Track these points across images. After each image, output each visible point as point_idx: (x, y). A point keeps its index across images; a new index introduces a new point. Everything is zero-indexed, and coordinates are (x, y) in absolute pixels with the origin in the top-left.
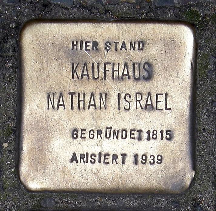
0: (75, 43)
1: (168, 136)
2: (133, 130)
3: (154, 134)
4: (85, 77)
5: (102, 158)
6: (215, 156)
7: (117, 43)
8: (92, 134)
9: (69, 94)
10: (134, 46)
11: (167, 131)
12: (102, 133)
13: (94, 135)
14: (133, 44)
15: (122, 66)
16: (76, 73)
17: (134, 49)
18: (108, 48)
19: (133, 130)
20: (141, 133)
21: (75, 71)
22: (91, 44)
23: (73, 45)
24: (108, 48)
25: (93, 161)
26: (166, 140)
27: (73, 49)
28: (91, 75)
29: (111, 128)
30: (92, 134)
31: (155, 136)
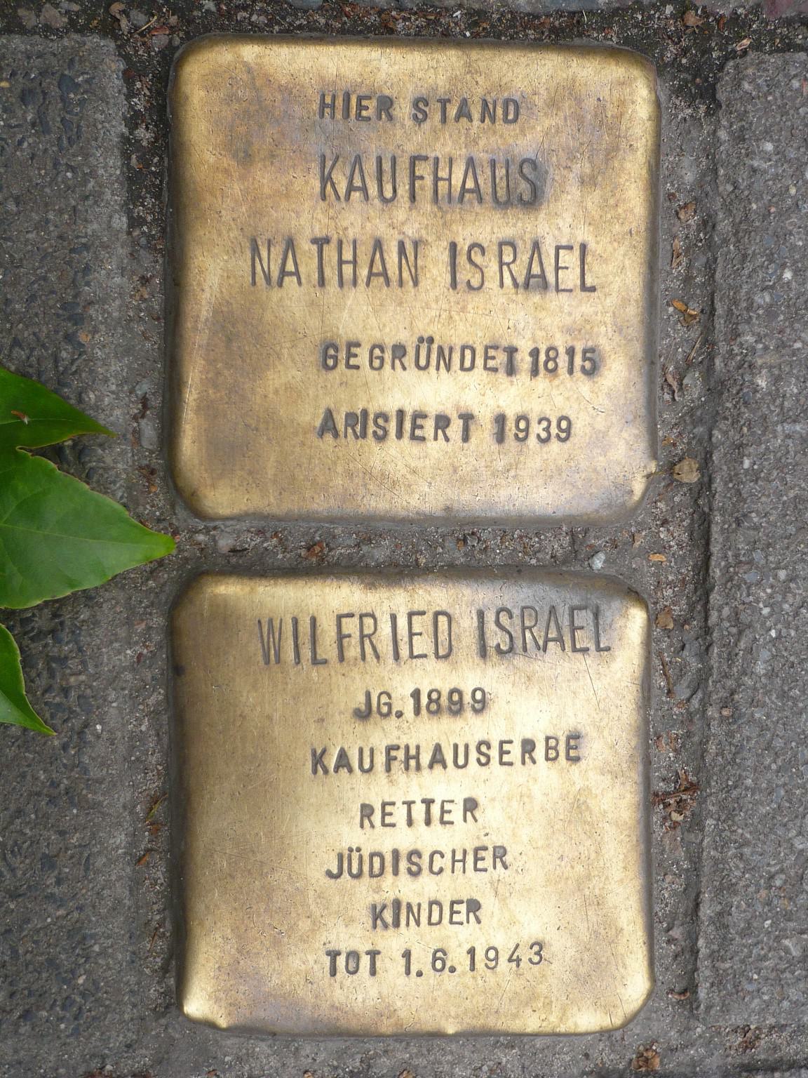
1: (588, 365)
3: (548, 359)
18: (420, 116)
24: (420, 116)
28: (373, 190)
29: (431, 340)
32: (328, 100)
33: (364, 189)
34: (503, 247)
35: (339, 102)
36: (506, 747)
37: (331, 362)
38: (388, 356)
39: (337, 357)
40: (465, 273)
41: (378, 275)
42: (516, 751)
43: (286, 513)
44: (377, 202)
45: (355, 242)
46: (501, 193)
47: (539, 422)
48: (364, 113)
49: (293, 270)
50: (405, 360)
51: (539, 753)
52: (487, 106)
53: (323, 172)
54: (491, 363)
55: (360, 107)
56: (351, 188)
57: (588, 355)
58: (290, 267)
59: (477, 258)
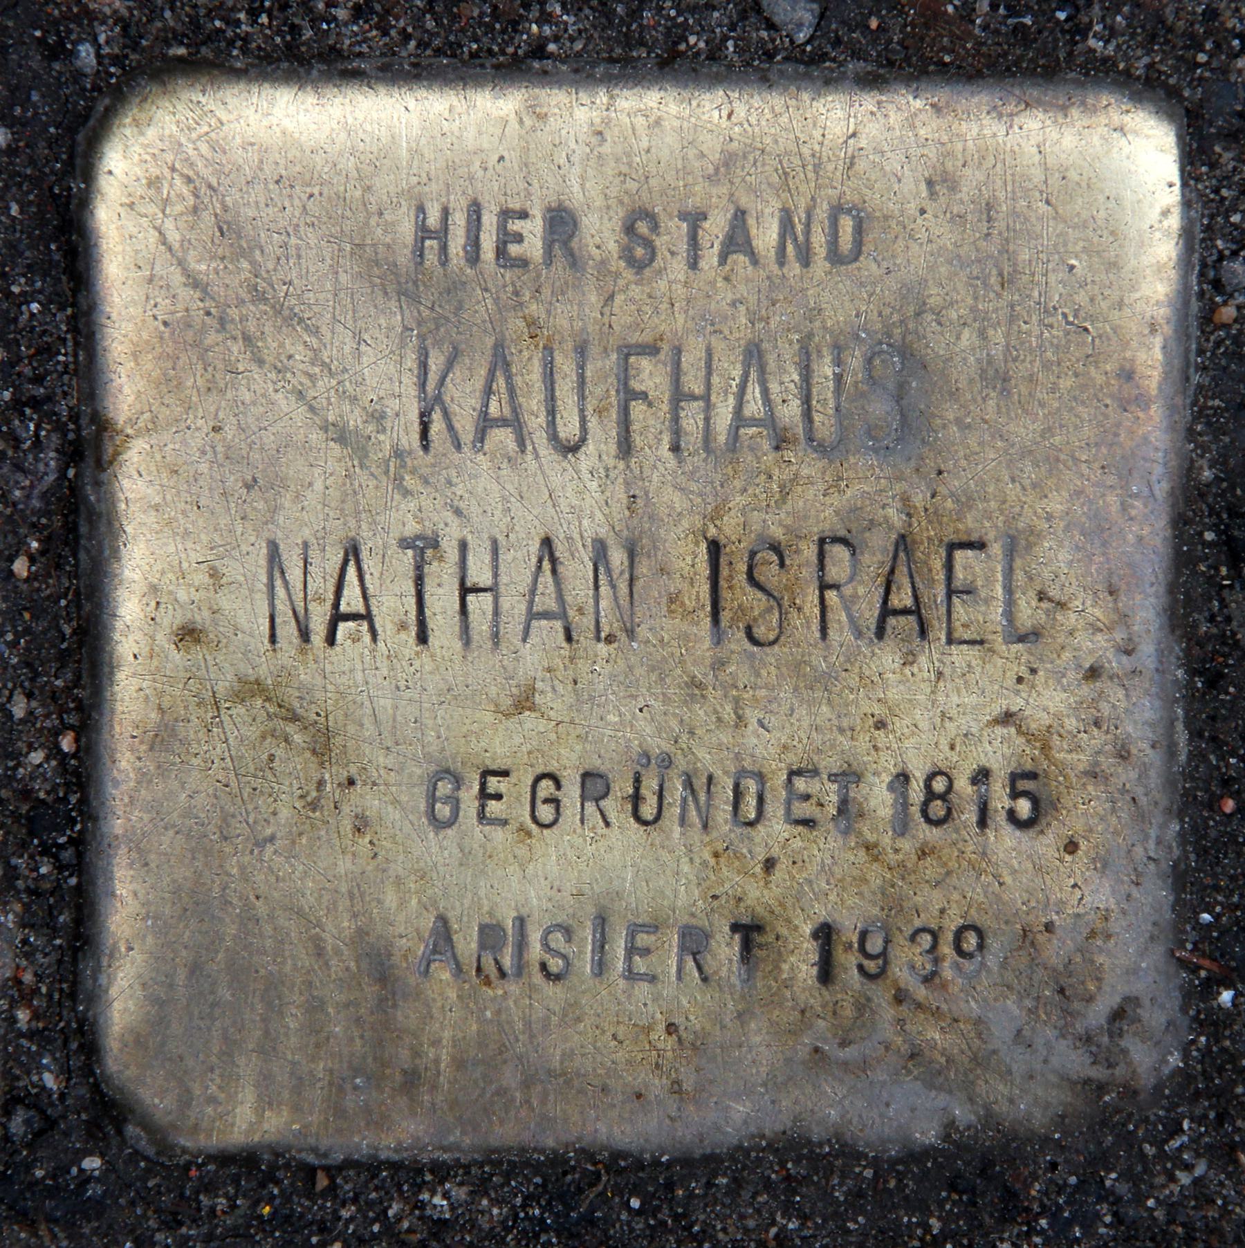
0: (433, 220)
1: (1024, 807)
2: (799, 773)
3: (931, 795)
4: (502, 437)
5: (461, 241)
6: (1242, 949)
7: (695, 219)
8: (546, 801)
9: (405, 543)
10: (801, 238)
11: (1014, 778)
12: (606, 795)
13: (554, 801)
14: (799, 228)
15: (731, 369)
16: (446, 414)
17: (805, 258)
18: (639, 252)
19: (799, 773)
20: (758, 938)
21: (438, 399)
22: (533, 231)
23: (423, 232)
24: (639, 252)
25: (555, 965)
26: (1008, 829)
27: (420, 252)
28: (536, 422)
29: (667, 762)
30: (546, 801)
31: (937, 809)
32: (433, 220)
33: (515, 422)
34: (827, 547)
35: (459, 220)
36: (493, 783)
37: (444, 811)
38: (571, 794)
39: (458, 800)
40: (739, 595)
41: (546, 615)
42: (515, 789)
43: (116, 575)
44: (546, 451)
45: (458, 447)
46: (824, 422)
47: (913, 938)
48: (514, 249)
49: (362, 611)
50: (608, 804)
51: (571, 794)
52: (793, 227)
53: (422, 385)
54: (803, 810)
55: (506, 238)
56: (485, 424)
57: (1023, 785)
58: (352, 600)
59: (770, 573)
